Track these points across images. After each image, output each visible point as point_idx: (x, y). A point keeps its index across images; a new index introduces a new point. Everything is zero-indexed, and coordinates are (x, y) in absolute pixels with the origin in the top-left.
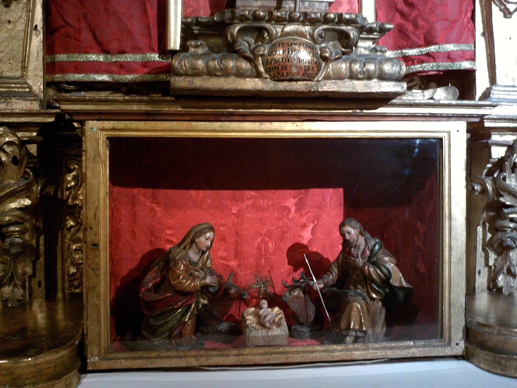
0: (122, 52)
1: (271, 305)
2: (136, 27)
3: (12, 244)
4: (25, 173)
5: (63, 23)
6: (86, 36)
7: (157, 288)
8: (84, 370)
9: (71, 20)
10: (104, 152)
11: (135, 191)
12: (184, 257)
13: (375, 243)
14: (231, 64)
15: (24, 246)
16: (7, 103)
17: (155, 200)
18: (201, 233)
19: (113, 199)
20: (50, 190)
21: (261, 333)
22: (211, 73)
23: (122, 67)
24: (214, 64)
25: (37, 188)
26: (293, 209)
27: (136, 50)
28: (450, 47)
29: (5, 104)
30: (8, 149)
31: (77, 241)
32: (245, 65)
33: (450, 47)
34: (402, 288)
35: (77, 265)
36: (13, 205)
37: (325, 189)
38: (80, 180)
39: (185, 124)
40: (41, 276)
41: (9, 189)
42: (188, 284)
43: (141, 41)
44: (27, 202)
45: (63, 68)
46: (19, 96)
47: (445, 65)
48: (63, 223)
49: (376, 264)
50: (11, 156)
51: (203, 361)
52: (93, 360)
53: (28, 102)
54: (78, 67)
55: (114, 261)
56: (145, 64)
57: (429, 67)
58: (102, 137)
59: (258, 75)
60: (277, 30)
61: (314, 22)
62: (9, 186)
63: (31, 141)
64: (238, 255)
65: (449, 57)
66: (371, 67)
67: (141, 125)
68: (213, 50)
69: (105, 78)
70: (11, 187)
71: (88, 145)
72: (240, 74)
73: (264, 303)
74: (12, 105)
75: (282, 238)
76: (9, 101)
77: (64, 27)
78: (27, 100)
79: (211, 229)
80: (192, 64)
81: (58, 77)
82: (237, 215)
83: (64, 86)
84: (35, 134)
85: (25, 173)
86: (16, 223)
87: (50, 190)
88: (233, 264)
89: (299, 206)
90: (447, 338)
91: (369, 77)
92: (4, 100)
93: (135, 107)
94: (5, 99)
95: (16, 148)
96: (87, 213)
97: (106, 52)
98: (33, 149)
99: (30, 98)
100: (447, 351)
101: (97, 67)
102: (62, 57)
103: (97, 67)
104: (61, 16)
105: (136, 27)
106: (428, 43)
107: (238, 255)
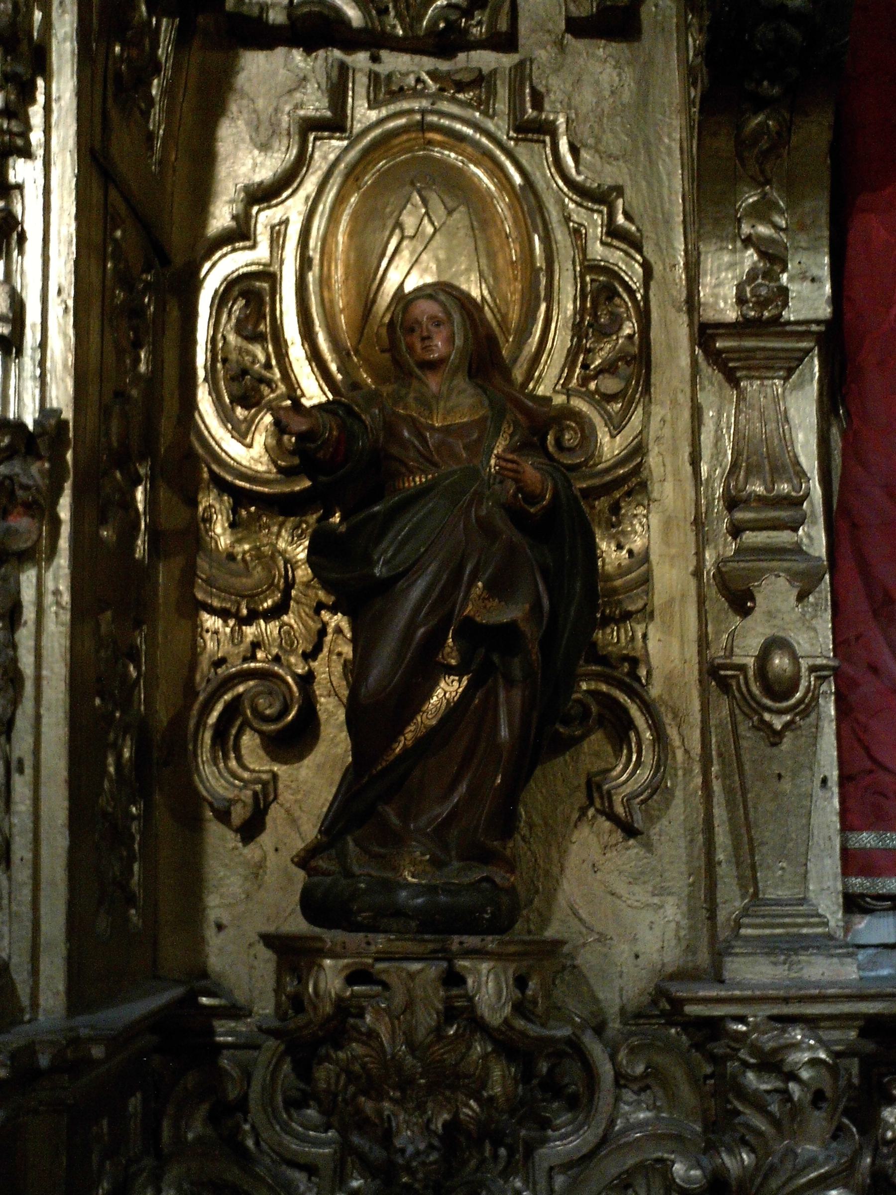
4: (840, 1128)
5: (868, 764)
16: (792, 964)
29: (786, 967)
30: (805, 1074)
41: (815, 1170)
46: (813, 948)
50: (813, 1089)
53: (835, 960)
62: (812, 1163)
70: (821, 1167)
74: (802, 969)
76: (794, 958)
77: (871, 771)
78: (832, 956)
80: (755, 500)
83: (868, 903)
84: (133, 911)
85: (840, 1128)
90: (577, 263)
92: (783, 958)
94: (785, 954)
95: (824, 1070)
99: (840, 951)
104: (867, 750)
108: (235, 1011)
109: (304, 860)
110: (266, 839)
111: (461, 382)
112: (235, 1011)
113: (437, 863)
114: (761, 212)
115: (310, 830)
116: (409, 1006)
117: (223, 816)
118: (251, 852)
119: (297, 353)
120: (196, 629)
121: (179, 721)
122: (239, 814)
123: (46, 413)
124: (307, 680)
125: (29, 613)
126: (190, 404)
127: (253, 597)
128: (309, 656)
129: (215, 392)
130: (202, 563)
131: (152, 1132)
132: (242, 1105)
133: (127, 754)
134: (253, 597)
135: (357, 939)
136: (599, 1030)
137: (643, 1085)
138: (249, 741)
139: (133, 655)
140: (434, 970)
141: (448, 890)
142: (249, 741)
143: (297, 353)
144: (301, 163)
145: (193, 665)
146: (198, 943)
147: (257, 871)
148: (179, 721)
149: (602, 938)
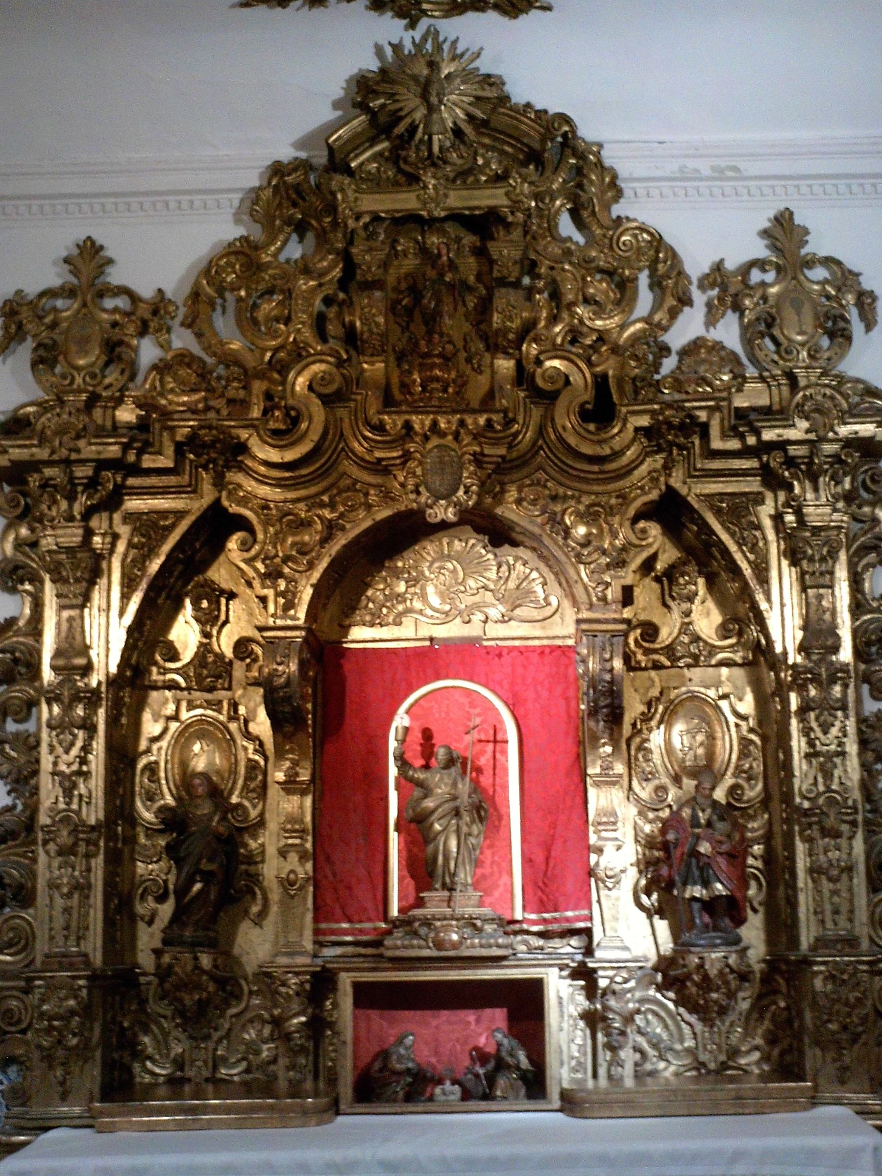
0: (360, 921)
1: (453, 1084)
2: (369, 905)
3: (296, 1045)
6: (338, 912)
7: (381, 1070)
8: (338, 1113)
9: (329, 901)
10: (349, 990)
11: (369, 1012)
12: (398, 1051)
13: (514, 1043)
14: (415, 942)
15: (302, 1046)
17: (382, 1017)
18: (406, 1037)
19: (355, 1018)
20: (317, 1011)
21: (443, 1098)
22: (405, 947)
23: (361, 931)
24: (406, 942)
25: (310, 1011)
26: (473, 1023)
27: (370, 920)
28: (570, 914)
31: (332, 1044)
32: (422, 943)
33: (570, 914)
34: (527, 1071)
35: (332, 1060)
36: (295, 1021)
37: (418, 1012)
38: (335, 1005)
39: (394, 973)
40: (311, 1067)
42: (399, 1067)
43: (372, 914)
44: (303, 1019)
45: (324, 933)
47: (566, 925)
48: (324, 1031)
49: (512, 1055)
51: (405, 1109)
52: (343, 1107)
54: (333, 932)
55: (356, 1058)
56: (375, 929)
57: (555, 927)
58: (348, 981)
59: (429, 948)
60: (438, 924)
61: (457, 920)
63: (307, 981)
64: (436, 1053)
65: (568, 920)
66: (492, 941)
67: (370, 974)
68: (407, 933)
69: (349, 938)
71: (340, 986)
72: (420, 947)
73: (448, 1083)
75: (466, 1043)
79: (412, 1034)
81: (321, 938)
82: (437, 1027)
86: (298, 1032)
87: (317, 1011)
88: (433, 1060)
89: (478, 1021)
91: (490, 946)
93: (366, 965)
96: (340, 1026)
97: (350, 921)
98: (307, 986)
100: (550, 1107)
101: (345, 932)
102: (323, 926)
103: (345, 932)
105: (369, 905)
106: (556, 911)
107: (436, 1053)
108: (145, 974)
109: (163, 931)
110: (155, 926)
111: (207, 800)
112: (145, 974)
113: (195, 931)
114: (291, 751)
115: (166, 921)
116: (185, 964)
117: (142, 919)
118: (150, 930)
119: (165, 788)
120: (135, 866)
121: (130, 892)
122: (147, 919)
123: (97, 820)
124: (165, 882)
125: (93, 869)
126: (133, 802)
127: (151, 857)
128: (167, 874)
129: (141, 798)
130: (137, 848)
131: (122, 1008)
132: (147, 1000)
133: (591, 157)
134: (151, 857)
135: (173, 948)
136: (246, 979)
137: (257, 993)
138: (150, 898)
139: (118, 875)
140: (192, 956)
141: (197, 937)
142: (150, 898)
143: (165, 788)
144: (165, 730)
145: (134, 877)
146: (134, 955)
147: (152, 936)
148: (130, 892)
149: (248, 953)
